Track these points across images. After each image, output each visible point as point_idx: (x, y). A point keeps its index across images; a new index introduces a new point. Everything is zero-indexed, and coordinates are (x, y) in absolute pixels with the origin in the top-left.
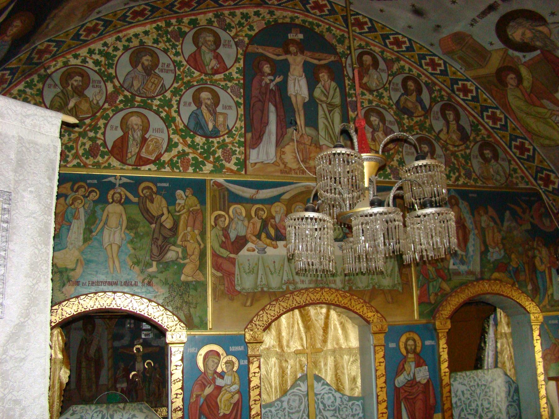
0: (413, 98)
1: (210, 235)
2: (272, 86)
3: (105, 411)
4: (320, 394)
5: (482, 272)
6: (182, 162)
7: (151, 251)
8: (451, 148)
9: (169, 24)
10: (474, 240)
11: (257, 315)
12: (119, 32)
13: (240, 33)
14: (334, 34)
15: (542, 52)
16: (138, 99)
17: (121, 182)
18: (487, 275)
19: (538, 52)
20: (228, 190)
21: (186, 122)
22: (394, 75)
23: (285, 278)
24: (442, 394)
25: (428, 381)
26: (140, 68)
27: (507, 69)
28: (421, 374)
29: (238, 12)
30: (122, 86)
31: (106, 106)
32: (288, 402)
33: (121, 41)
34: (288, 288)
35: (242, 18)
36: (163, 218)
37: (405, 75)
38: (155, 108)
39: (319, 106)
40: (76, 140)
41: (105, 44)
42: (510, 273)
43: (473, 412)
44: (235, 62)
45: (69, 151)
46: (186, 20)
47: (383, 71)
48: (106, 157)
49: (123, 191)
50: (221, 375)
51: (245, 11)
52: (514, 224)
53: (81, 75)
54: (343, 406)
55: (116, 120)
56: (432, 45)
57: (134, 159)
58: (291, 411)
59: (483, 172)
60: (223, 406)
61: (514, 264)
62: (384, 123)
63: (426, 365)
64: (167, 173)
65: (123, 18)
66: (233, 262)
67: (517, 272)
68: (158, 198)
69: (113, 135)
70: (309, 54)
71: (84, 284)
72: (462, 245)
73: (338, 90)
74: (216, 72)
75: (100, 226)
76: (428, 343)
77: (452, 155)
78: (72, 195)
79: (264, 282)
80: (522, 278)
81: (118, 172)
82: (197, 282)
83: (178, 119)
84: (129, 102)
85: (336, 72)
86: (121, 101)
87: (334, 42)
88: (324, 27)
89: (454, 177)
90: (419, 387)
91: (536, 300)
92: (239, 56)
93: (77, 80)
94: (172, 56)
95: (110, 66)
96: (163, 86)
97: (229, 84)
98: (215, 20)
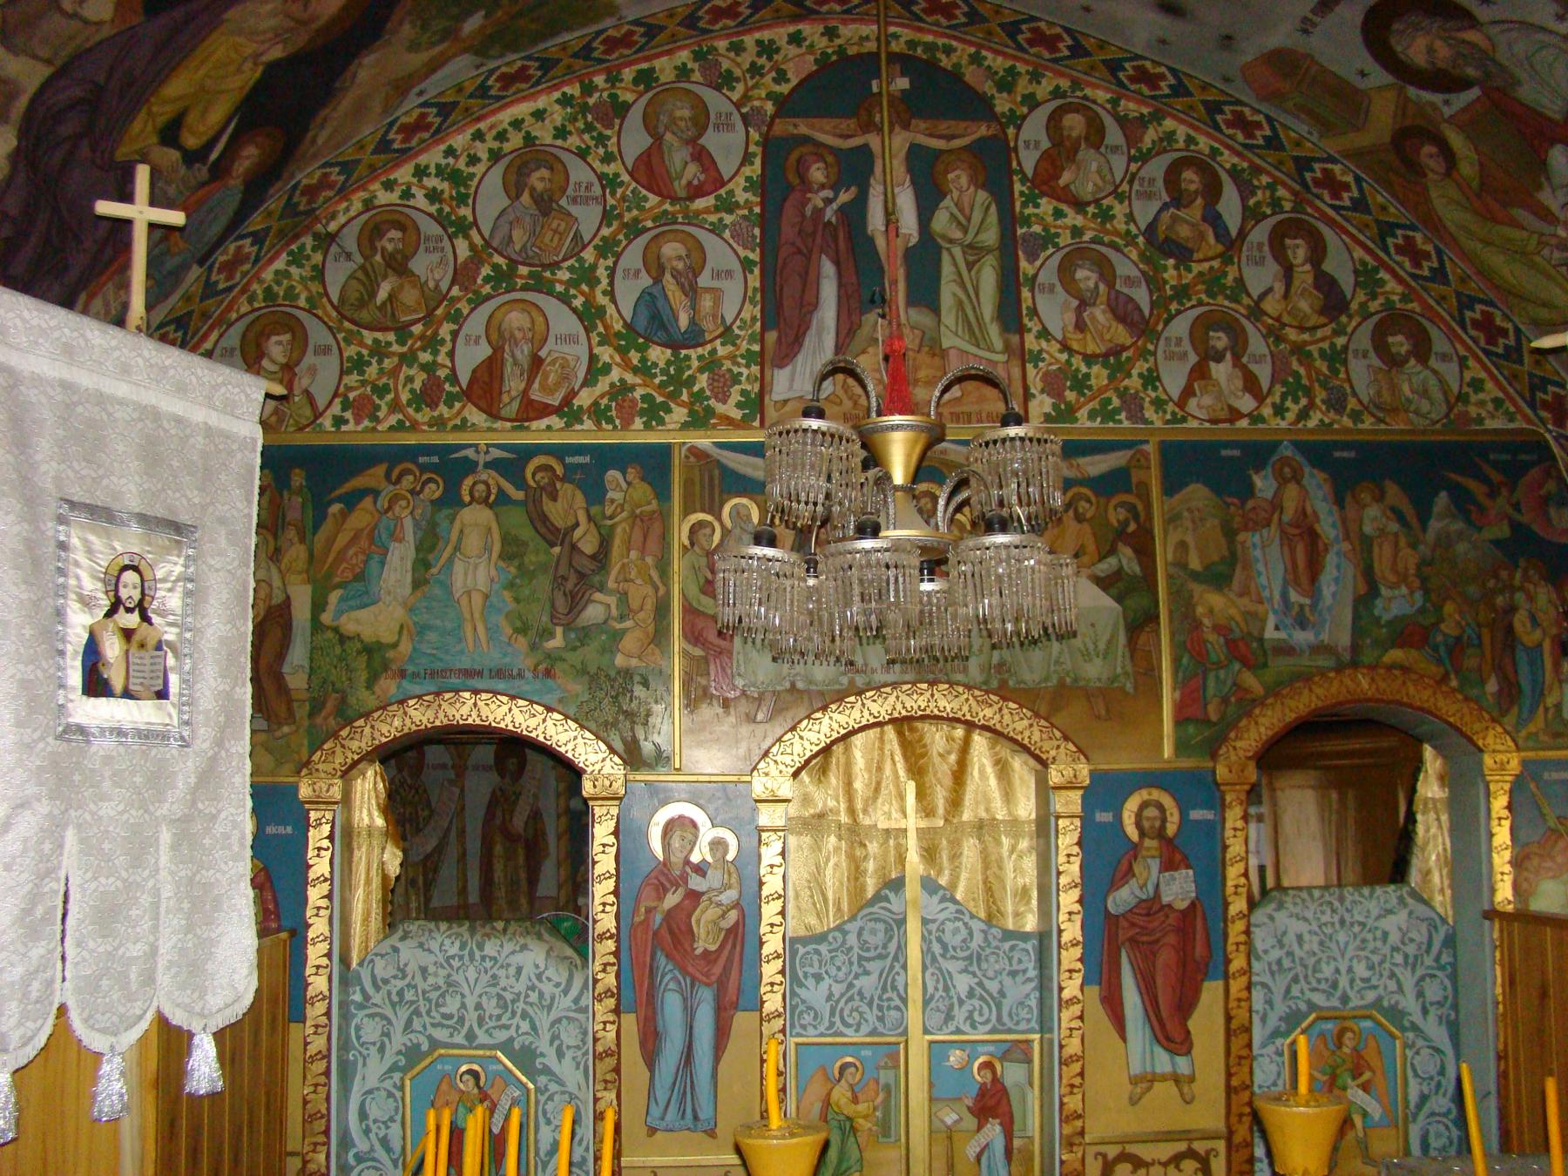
3: (467, 936)
5: (1355, 648)
10: (1338, 567)
25: (1193, 904)
32: (860, 934)
43: (1323, 986)
63: (1188, 867)
72: (1304, 580)
76: (1196, 814)
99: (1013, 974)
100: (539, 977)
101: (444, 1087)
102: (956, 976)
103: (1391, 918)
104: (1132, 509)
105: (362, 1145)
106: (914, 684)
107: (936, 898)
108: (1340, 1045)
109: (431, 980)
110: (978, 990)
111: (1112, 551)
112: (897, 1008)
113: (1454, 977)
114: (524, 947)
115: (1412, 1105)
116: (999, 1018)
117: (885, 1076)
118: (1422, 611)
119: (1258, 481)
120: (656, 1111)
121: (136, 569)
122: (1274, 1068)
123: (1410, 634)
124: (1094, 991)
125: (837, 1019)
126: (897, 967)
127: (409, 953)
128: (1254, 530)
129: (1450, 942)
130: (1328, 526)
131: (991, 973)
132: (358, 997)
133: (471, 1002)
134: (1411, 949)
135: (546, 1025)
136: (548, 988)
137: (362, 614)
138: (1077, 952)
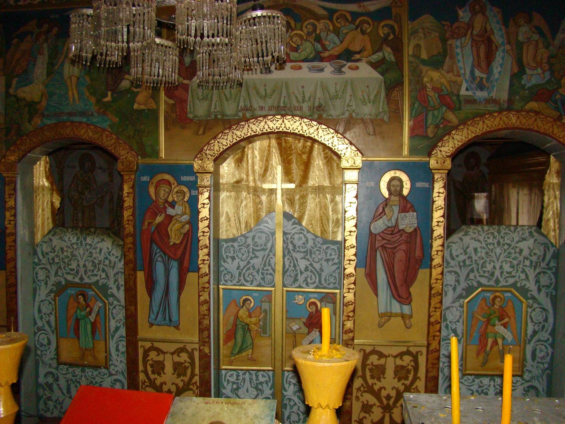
3: (79, 234)
4: (289, 234)
5: (510, 101)
10: (503, 58)
23: (242, 104)
24: (431, 247)
25: (415, 230)
28: (407, 221)
32: (253, 239)
34: (244, 115)
43: (486, 274)
54: (315, 249)
58: (256, 248)
60: (173, 236)
72: (483, 64)
76: (419, 185)
90: (401, 236)
99: (327, 260)
100: (109, 253)
101: (71, 301)
103: (524, 242)
104: (392, 28)
105: (40, 324)
106: (274, 116)
107: (291, 223)
108: (494, 304)
109: (65, 254)
110: (310, 268)
111: (380, 49)
112: (271, 274)
113: (556, 274)
114: (103, 240)
115: (112, 332)
117: (265, 306)
118: (549, 82)
119: (461, 13)
120: (153, 317)
122: (458, 313)
123: (541, 94)
124: (362, 271)
125: (242, 278)
126: (271, 256)
128: (457, 39)
129: (556, 256)
130: (498, 37)
131: (316, 260)
132: (36, 260)
133: (81, 264)
134: (534, 258)
135: (112, 275)
136: (113, 258)
137: (27, 89)
138: (353, 251)
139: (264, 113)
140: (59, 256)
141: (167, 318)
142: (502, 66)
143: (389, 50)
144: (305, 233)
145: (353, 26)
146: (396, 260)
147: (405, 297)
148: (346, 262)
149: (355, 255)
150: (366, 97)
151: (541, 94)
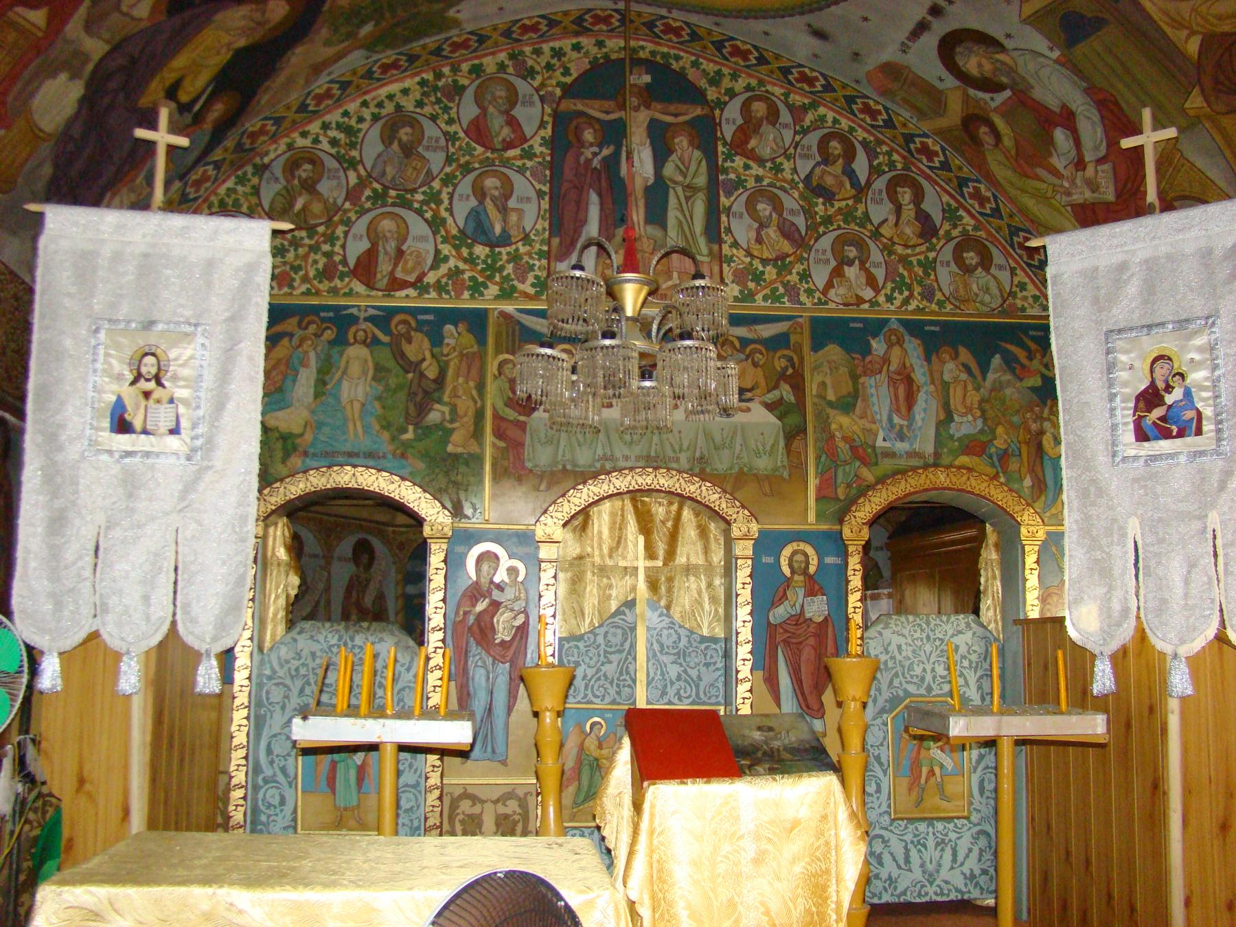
0: (838, 168)
1: (491, 388)
2: (596, 163)
3: (343, 632)
5: (937, 455)
6: (454, 284)
7: (407, 408)
8: (900, 250)
9: (439, 76)
10: (926, 401)
11: (554, 502)
12: (366, 93)
13: (548, 82)
14: (704, 70)
15: (1014, 94)
16: (393, 193)
17: (367, 315)
18: (946, 460)
19: (1007, 94)
20: (519, 323)
21: (461, 225)
22: (805, 132)
23: (600, 452)
26: (395, 146)
27: (973, 121)
28: (815, 608)
29: (546, 47)
30: (369, 175)
31: (347, 205)
33: (368, 107)
34: (603, 466)
35: (553, 57)
36: (425, 365)
37: (826, 131)
38: (416, 205)
39: (671, 191)
40: (306, 256)
41: (346, 114)
42: (991, 457)
43: (915, 680)
44: (539, 128)
45: (296, 273)
46: (465, 67)
47: (786, 126)
48: (347, 280)
49: (368, 326)
50: (500, 587)
51: (557, 44)
52: (1008, 377)
53: (312, 162)
55: (361, 226)
56: (857, 82)
57: (385, 281)
59: (957, 290)
61: (999, 443)
62: (780, 215)
63: (823, 594)
64: (431, 301)
65: (369, 75)
66: (522, 426)
67: (1004, 456)
68: (417, 336)
69: (356, 248)
70: (659, 107)
71: (314, 455)
73: (704, 163)
74: (509, 145)
75: (337, 376)
76: (829, 560)
77: (900, 261)
78: (299, 333)
79: (568, 456)
80: (1013, 465)
81: (362, 299)
82: (470, 454)
83: (450, 221)
84: (379, 197)
85: (705, 133)
86: (368, 198)
87: (703, 83)
88: (687, 59)
89: (899, 298)
91: (1039, 505)
92: (546, 118)
93: (305, 170)
94: (443, 125)
95: (353, 145)
96: (429, 172)
97: (529, 164)
98: (510, 63)
99: (707, 665)
102: (669, 666)
104: (790, 360)
105: (268, 772)
106: (644, 468)
107: (657, 614)
109: (318, 661)
111: (776, 387)
112: (629, 686)
114: (381, 640)
116: (697, 695)
118: (982, 431)
119: (874, 344)
121: (153, 354)
122: (881, 734)
123: (974, 447)
124: (760, 674)
125: (589, 692)
127: (304, 643)
130: (920, 374)
137: (280, 414)
139: (629, 464)
140: (307, 665)
141: (489, 749)
142: (926, 409)
143: (787, 387)
144: (677, 627)
145: (743, 356)
146: (803, 658)
147: (816, 708)
148: (739, 663)
149: (750, 652)
150: (761, 448)
151: (974, 447)
